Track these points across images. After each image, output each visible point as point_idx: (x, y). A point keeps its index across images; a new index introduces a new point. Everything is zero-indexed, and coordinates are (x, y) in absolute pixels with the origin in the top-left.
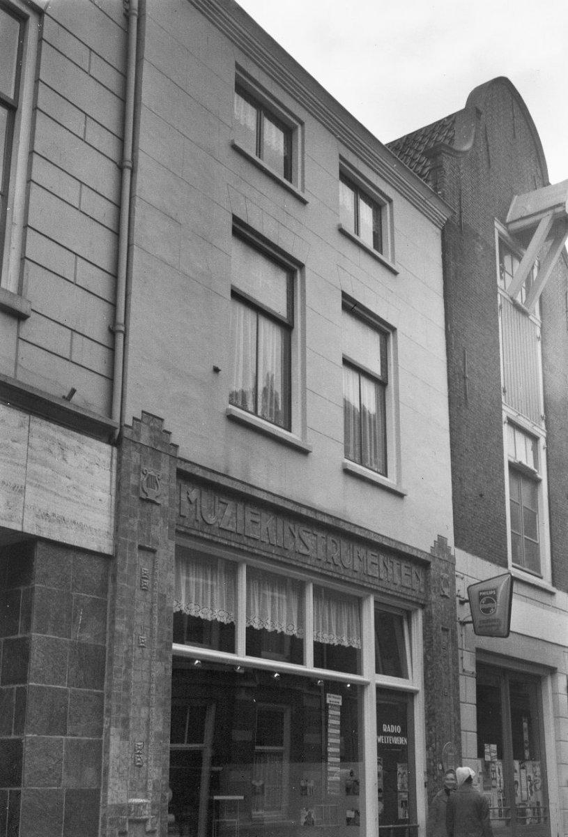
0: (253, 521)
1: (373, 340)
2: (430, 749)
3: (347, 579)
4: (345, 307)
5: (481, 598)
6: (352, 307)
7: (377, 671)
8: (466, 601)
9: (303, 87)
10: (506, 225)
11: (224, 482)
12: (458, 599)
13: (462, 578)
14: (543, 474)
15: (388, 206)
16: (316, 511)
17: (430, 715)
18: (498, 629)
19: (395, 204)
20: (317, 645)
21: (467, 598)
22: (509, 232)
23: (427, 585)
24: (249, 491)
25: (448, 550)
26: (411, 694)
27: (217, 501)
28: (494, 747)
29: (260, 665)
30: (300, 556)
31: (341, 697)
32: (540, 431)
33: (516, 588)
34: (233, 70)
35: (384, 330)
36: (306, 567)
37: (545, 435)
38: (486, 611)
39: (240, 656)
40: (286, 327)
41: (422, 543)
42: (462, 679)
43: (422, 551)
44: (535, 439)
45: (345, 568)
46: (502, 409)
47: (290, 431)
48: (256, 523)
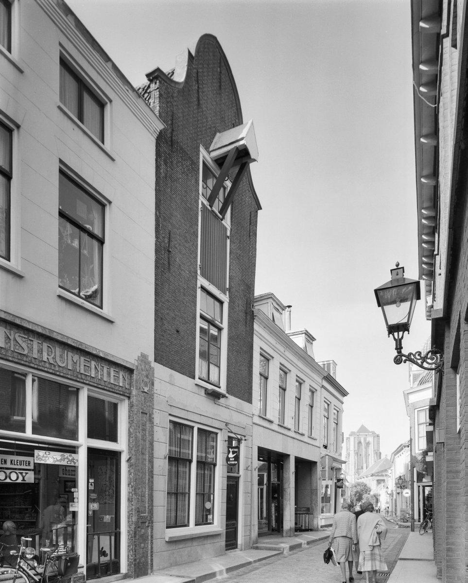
2: (130, 486)
7: (32, 434)
15: (109, 105)
23: (130, 384)
25: (149, 363)
32: (225, 298)
39: (29, 433)
40: (101, 242)
41: (129, 358)
44: (221, 303)
47: (10, 261)
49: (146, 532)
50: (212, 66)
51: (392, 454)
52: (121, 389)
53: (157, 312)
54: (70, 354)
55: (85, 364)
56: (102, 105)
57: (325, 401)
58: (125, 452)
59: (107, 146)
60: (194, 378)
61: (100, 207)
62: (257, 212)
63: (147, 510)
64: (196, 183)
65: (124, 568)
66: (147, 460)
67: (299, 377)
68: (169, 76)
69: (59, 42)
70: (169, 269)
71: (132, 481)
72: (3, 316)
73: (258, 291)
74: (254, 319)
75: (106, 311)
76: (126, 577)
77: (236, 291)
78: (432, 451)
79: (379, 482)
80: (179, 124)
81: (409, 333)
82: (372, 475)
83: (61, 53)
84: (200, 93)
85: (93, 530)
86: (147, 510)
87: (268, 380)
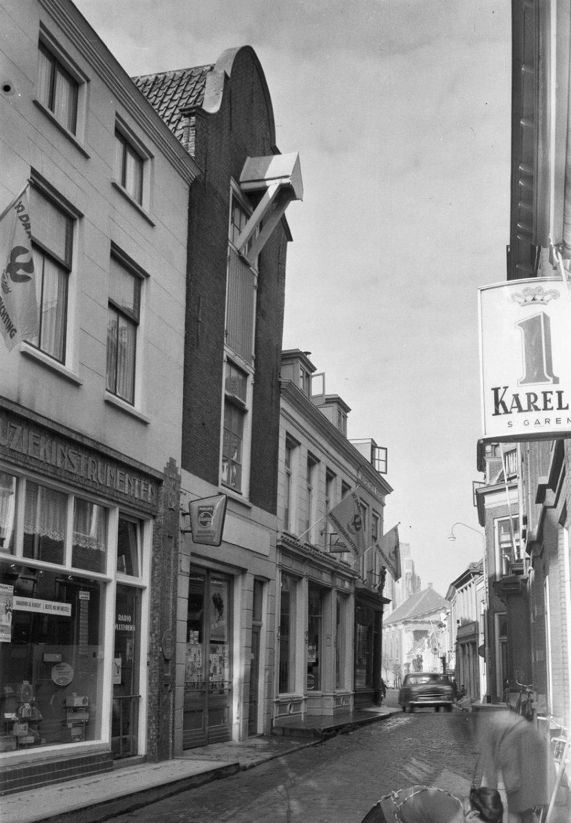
0: (34, 443)
1: (128, 283)
2: (153, 635)
3: (101, 494)
4: (113, 256)
5: (200, 512)
6: (118, 256)
8: (187, 514)
9: (120, 83)
10: (239, 183)
11: (17, 410)
12: (181, 512)
13: (185, 494)
14: (249, 405)
15: (86, 85)
16: (83, 436)
17: (154, 607)
18: (212, 539)
19: (156, 158)
20: (76, 549)
21: (188, 511)
22: (241, 190)
23: (157, 499)
24: (34, 418)
25: (176, 469)
26: (141, 589)
27: (9, 425)
28: (197, 633)
29: (80, 574)
30: (67, 473)
31: (89, 593)
32: (250, 370)
33: (230, 505)
34: (37, 29)
35: (139, 276)
36: (72, 483)
38: (204, 523)
39: (67, 566)
40: (65, 269)
41: (157, 464)
42: (179, 578)
43: (157, 471)
44: (246, 375)
45: (100, 484)
46: (223, 349)
47: (64, 365)
48: (37, 445)
49: (168, 700)
51: (452, 584)
52: (149, 507)
53: (185, 400)
54: (61, 447)
55: (35, 441)
58: (148, 588)
60: (216, 484)
61: (63, 222)
65: (142, 749)
67: (291, 436)
71: (157, 628)
72: (5, 405)
75: (138, 408)
76: (145, 760)
79: (419, 635)
81: (493, 415)
82: (406, 623)
83: (40, 34)
85: (333, 685)
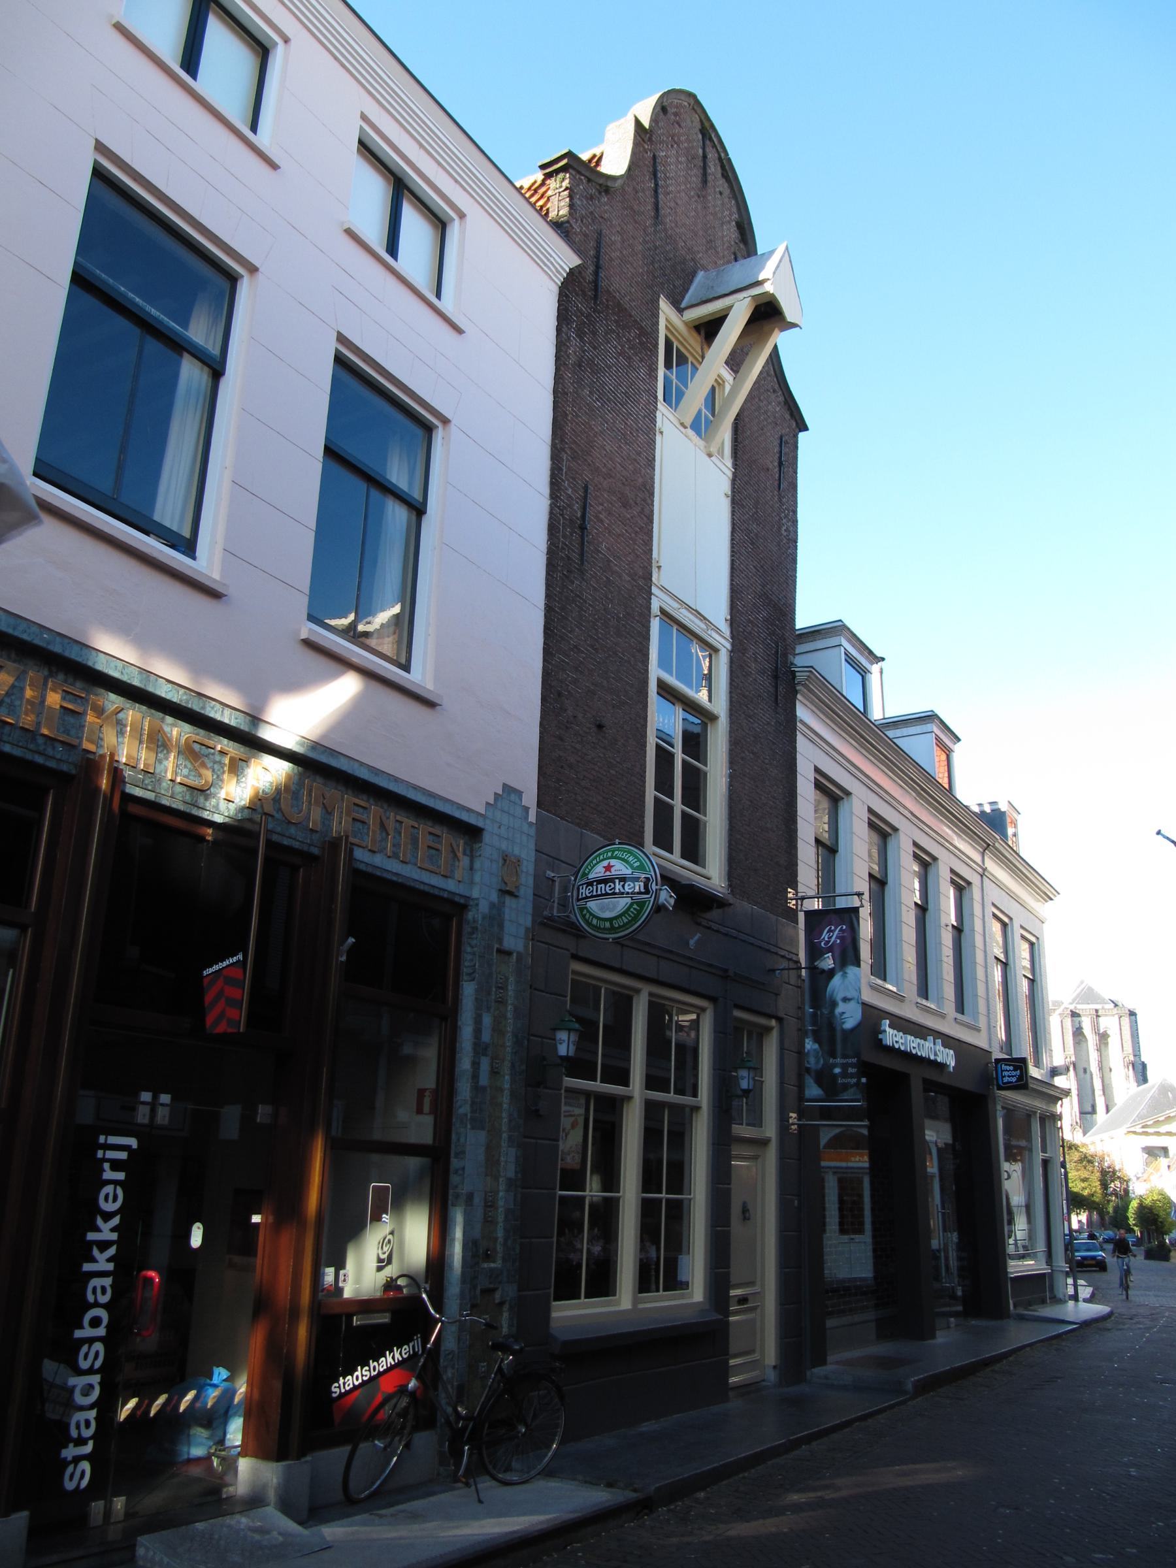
22: (686, 324)
37: (729, 646)
50: (686, 145)
56: (440, 224)
57: (995, 916)
59: (447, 304)
62: (796, 437)
63: (499, 1248)
64: (650, 375)
66: (507, 1093)
68: (593, 165)
69: (362, 112)
70: (582, 572)
73: (804, 619)
74: (796, 692)
77: (750, 621)
78: (809, 914)
80: (613, 255)
84: (661, 196)
86: (499, 1248)
87: (837, 856)
